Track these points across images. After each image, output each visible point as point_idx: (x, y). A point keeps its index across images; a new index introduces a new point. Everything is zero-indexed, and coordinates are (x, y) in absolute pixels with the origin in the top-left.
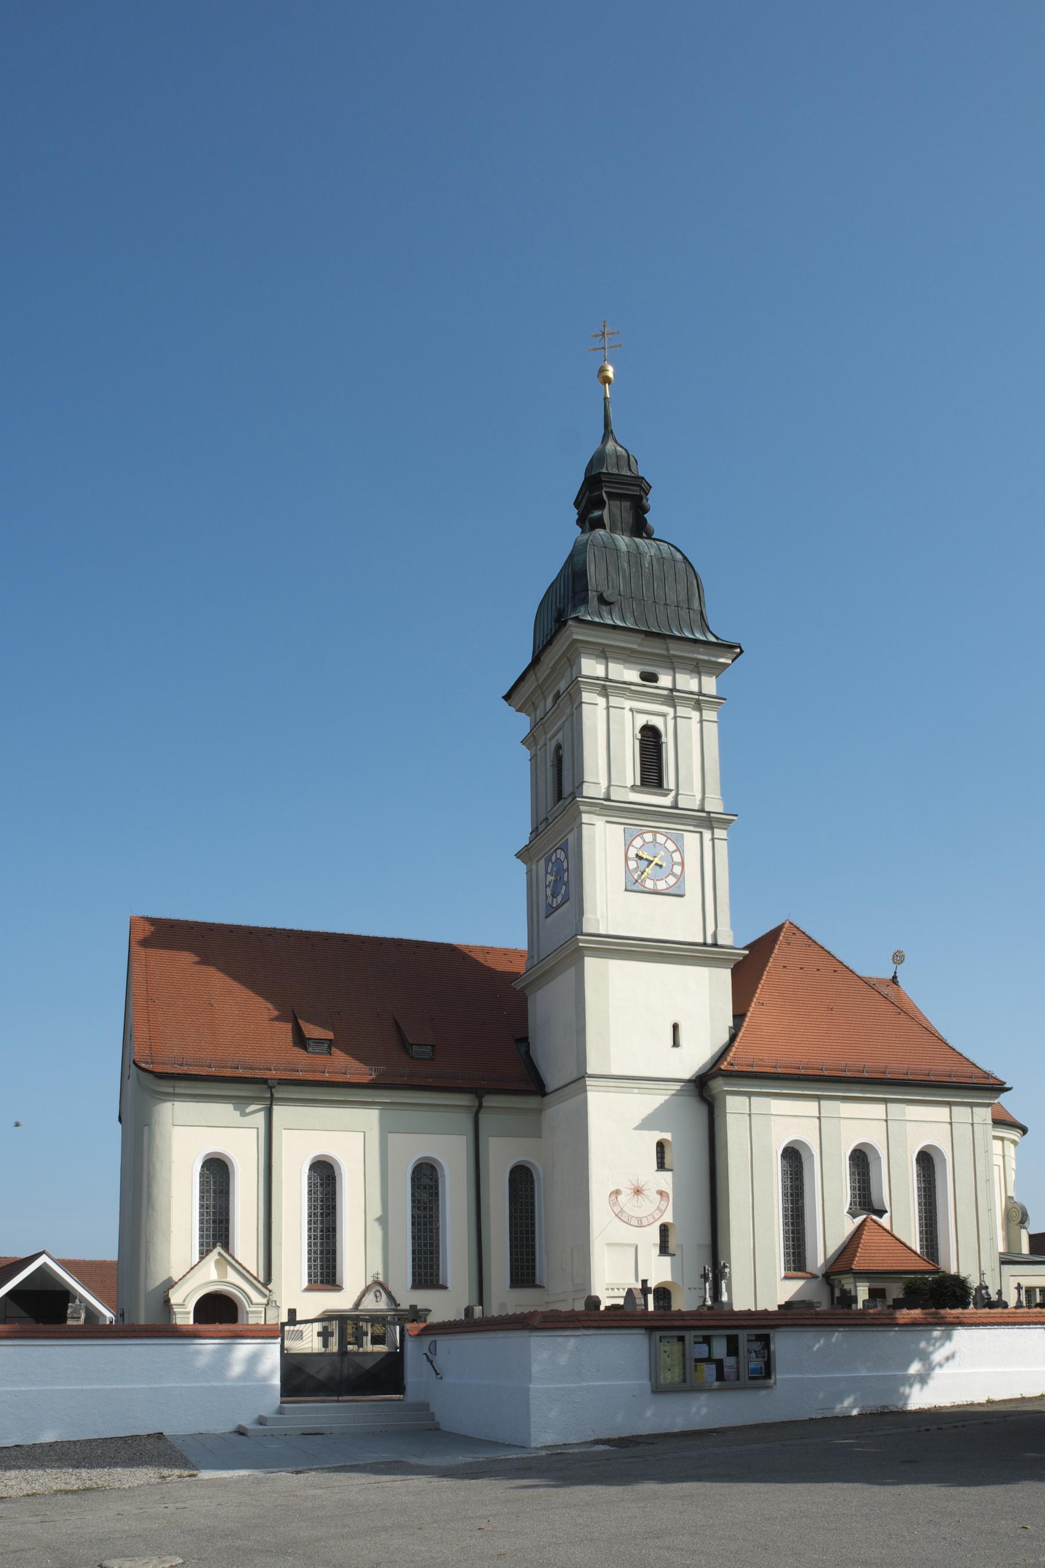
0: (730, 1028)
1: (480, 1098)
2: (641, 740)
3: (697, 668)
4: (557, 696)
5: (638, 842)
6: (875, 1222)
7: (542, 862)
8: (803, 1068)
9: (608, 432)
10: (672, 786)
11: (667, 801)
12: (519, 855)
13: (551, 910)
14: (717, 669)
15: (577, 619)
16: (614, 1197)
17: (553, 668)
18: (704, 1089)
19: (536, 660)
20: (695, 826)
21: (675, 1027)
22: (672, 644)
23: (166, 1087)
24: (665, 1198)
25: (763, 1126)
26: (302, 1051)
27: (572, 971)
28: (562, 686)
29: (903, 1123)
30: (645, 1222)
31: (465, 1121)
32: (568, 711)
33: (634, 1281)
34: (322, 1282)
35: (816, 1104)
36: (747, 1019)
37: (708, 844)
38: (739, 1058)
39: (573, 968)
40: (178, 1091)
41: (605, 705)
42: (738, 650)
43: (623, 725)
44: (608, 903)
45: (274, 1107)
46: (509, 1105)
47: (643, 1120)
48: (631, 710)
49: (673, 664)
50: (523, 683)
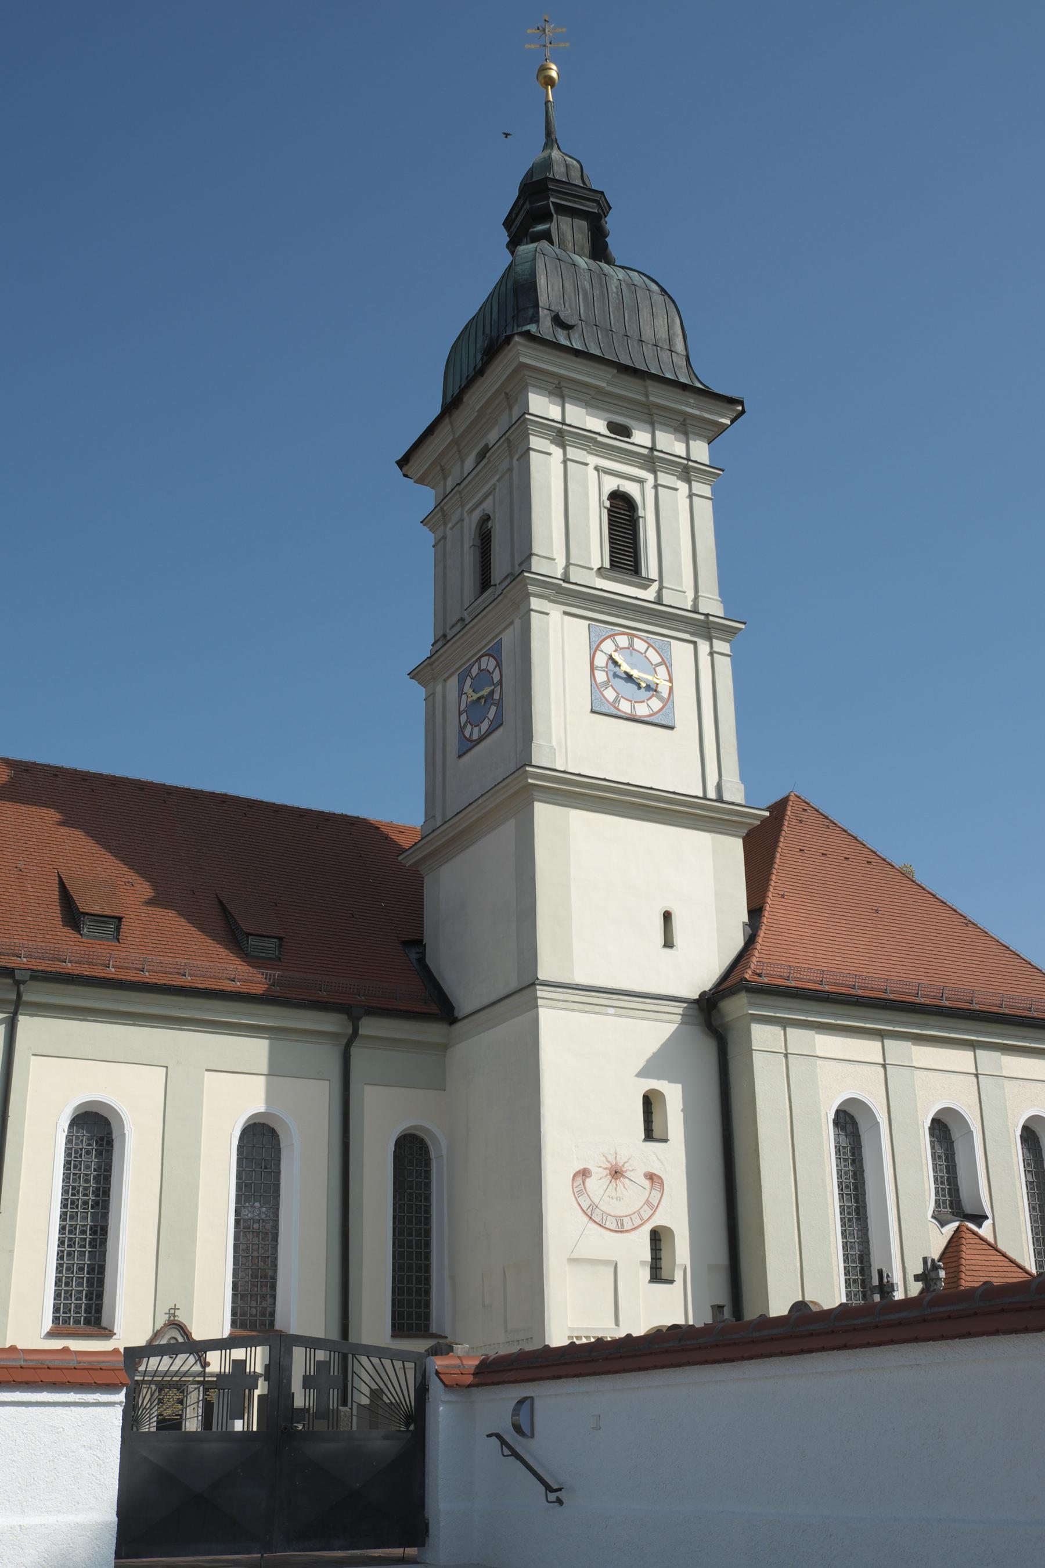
0: (745, 924)
1: (355, 1020)
2: (609, 510)
3: (684, 428)
4: (482, 454)
5: (608, 646)
6: (974, 1233)
7: (454, 681)
8: (860, 988)
9: (550, 140)
10: (654, 574)
11: (650, 594)
12: (414, 674)
13: (467, 745)
14: (713, 433)
15: (528, 335)
16: (579, 1181)
17: (482, 412)
18: (712, 1018)
19: (451, 405)
20: (692, 634)
21: (667, 916)
22: (652, 387)
24: (657, 1186)
25: (807, 1075)
26: (71, 933)
27: (508, 829)
28: (492, 437)
29: (1000, 1080)
30: (627, 1227)
31: (329, 1057)
32: (505, 466)
33: (613, 1325)
34: (88, 1322)
35: (879, 1044)
36: (766, 914)
38: (770, 963)
39: (511, 824)
41: (561, 458)
42: (740, 408)
43: (585, 486)
44: (569, 725)
45: (20, 1018)
46: (397, 1035)
47: (648, 1061)
48: (597, 468)
49: (653, 417)
50: (431, 438)
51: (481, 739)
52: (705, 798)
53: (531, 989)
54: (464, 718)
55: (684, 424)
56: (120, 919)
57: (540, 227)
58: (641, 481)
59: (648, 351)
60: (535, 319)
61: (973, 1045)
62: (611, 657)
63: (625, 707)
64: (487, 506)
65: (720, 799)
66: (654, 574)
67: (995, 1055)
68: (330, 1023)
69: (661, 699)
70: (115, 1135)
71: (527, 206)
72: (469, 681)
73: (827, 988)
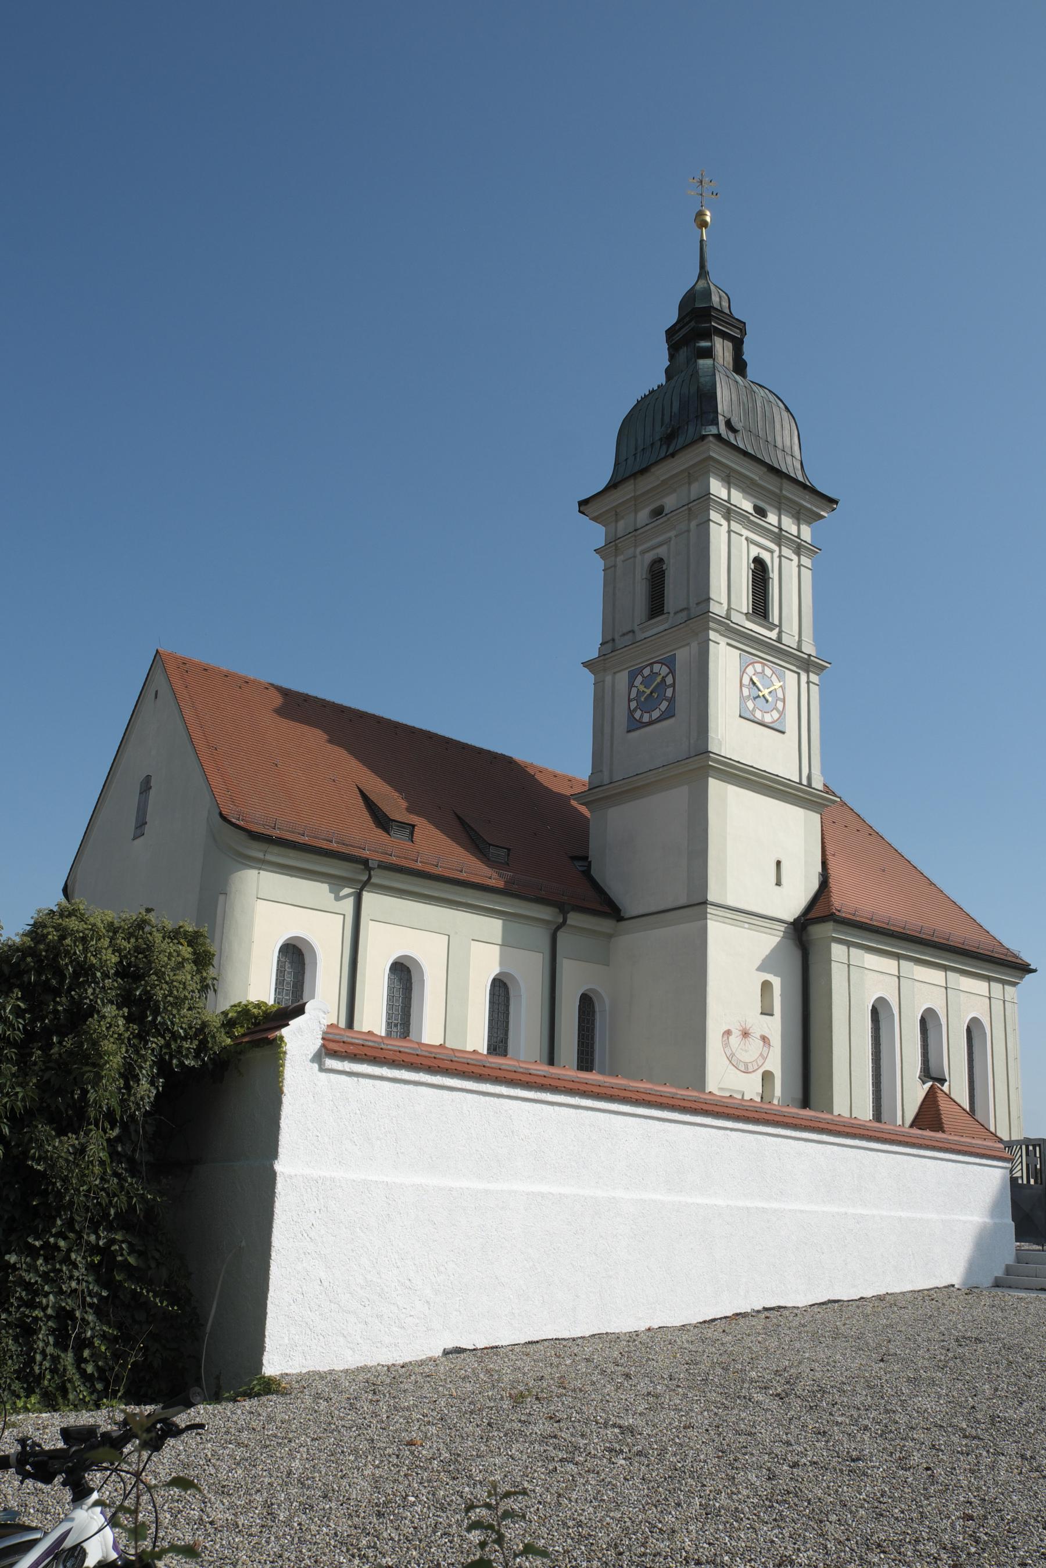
5: (750, 670)
7: (623, 677)
9: (703, 273)
10: (776, 622)
11: (774, 635)
13: (635, 725)
17: (664, 482)
20: (798, 667)
21: (779, 863)
23: (256, 850)
26: (385, 834)
31: (541, 936)
37: (804, 686)
39: (685, 789)
40: (269, 857)
43: (741, 551)
45: (364, 893)
47: (763, 961)
48: (747, 539)
49: (782, 505)
51: (651, 723)
52: (800, 783)
53: (703, 906)
54: (633, 704)
55: (798, 513)
56: (413, 826)
57: (704, 344)
58: (772, 552)
59: (780, 454)
60: (716, 423)
61: (945, 968)
62: (751, 679)
63: (758, 715)
64: (661, 552)
65: (809, 785)
66: (776, 622)
67: (911, 964)
68: (545, 913)
69: (778, 711)
70: (307, 961)
71: (693, 324)
72: (639, 679)
73: (875, 923)
